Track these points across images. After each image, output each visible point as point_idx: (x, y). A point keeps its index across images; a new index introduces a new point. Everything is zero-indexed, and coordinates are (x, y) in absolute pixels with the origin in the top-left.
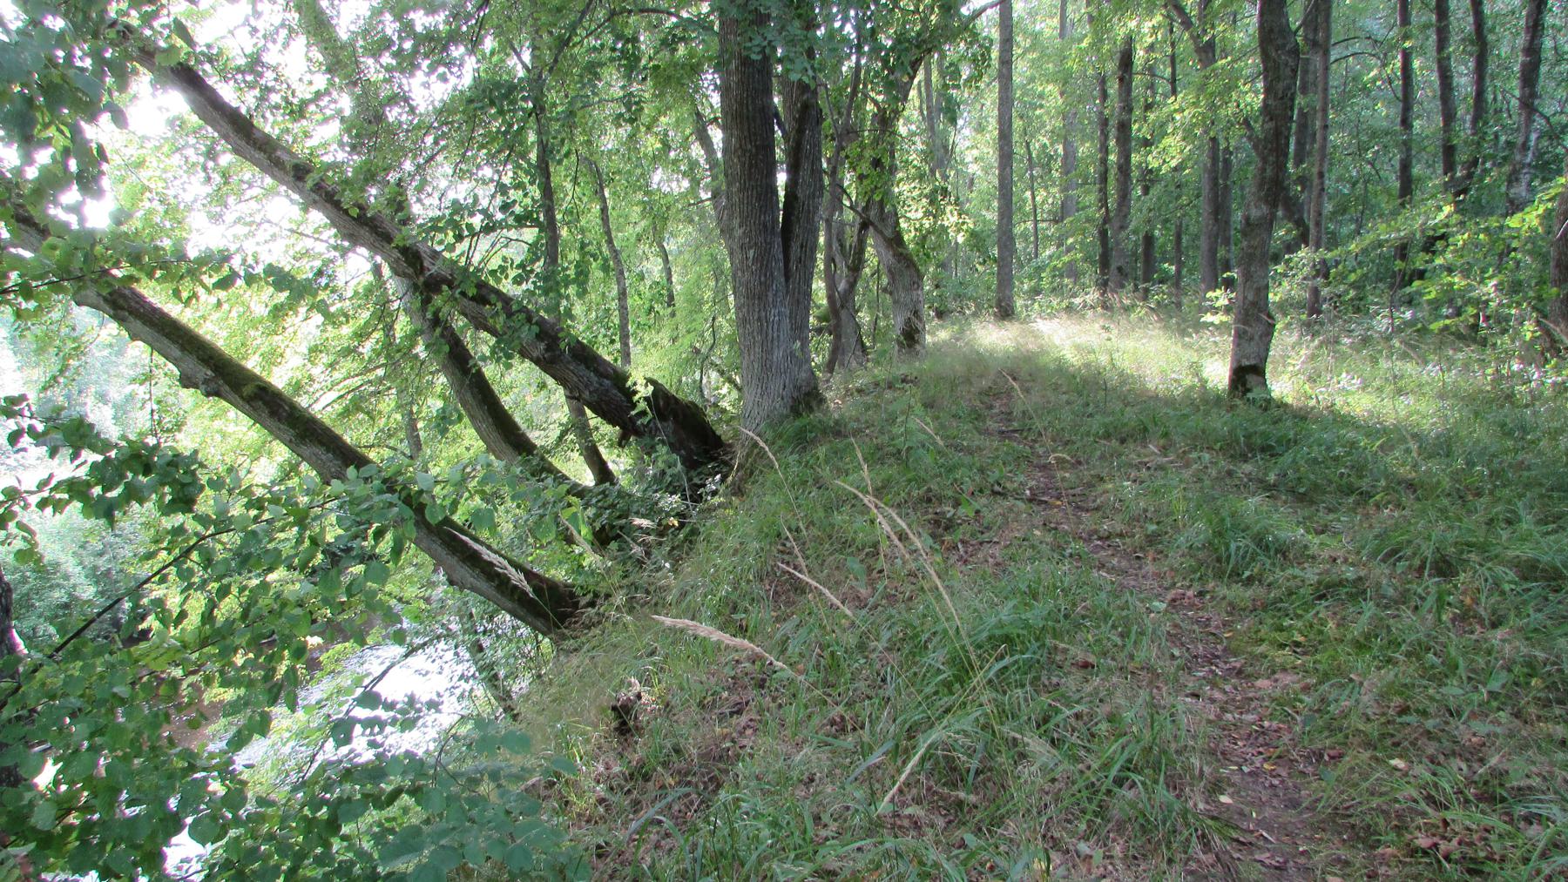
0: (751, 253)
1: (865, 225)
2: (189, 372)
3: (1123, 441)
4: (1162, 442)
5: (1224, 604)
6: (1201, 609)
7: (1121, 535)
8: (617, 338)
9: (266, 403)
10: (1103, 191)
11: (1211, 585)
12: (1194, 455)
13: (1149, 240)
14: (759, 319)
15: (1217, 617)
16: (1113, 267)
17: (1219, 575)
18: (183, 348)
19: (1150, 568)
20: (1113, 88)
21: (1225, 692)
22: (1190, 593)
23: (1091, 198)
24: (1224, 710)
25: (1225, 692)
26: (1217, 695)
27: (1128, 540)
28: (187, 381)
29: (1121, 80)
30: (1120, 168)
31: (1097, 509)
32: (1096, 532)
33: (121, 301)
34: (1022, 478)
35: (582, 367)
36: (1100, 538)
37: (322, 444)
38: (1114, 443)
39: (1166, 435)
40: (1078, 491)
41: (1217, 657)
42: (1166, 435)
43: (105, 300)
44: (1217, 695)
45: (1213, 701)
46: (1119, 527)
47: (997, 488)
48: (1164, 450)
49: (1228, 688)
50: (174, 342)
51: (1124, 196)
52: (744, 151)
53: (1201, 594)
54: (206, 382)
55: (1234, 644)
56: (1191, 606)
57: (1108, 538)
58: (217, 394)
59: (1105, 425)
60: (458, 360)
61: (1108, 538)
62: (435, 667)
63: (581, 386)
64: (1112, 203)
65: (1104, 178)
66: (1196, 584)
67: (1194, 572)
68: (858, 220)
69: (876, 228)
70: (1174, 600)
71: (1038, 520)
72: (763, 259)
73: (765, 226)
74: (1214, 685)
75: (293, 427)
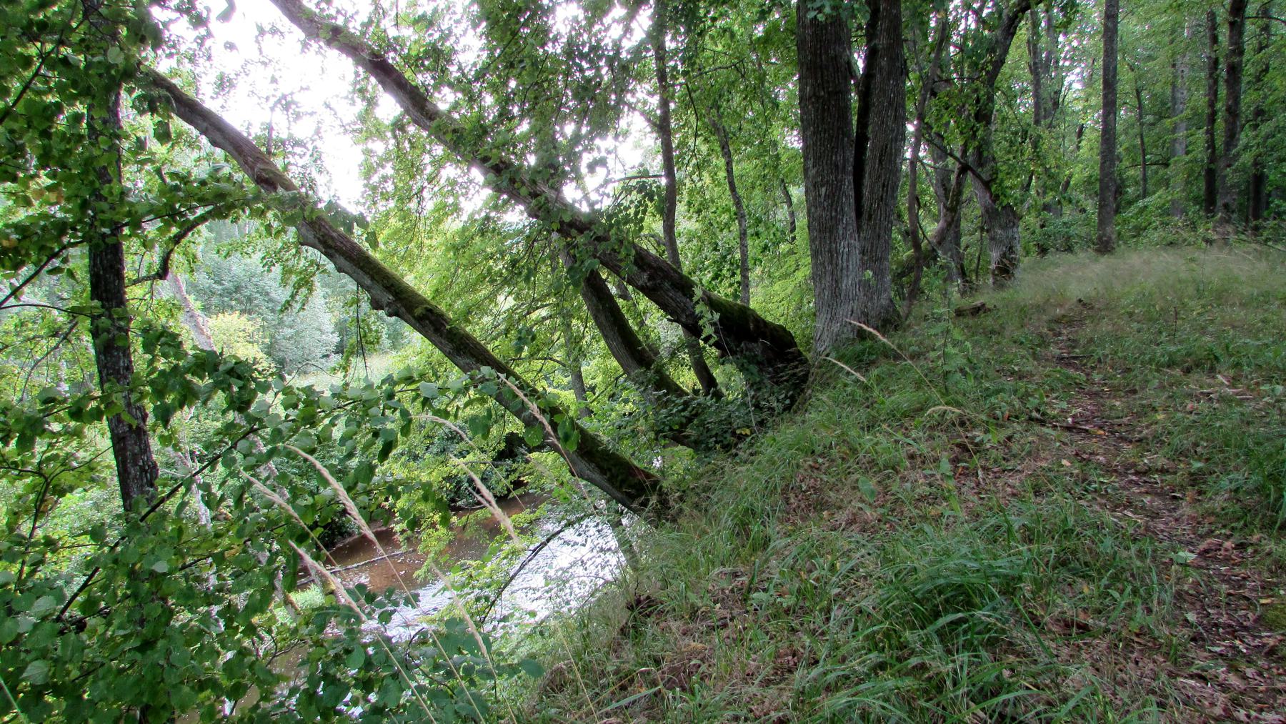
0: (823, 190)
1: (964, 169)
2: (378, 297)
3: (1188, 371)
4: (1232, 372)
5: (1268, 561)
6: (1238, 565)
7: (1163, 471)
8: (738, 272)
9: (431, 322)
10: (1210, 133)
11: (1256, 536)
12: (1266, 387)
13: (1259, 180)
14: (830, 251)
15: (1255, 575)
16: (1220, 203)
17: (1268, 526)
18: (372, 278)
19: (1186, 510)
20: (1224, 34)
21: (1244, 678)
22: (1228, 544)
23: (1201, 135)
24: (1236, 703)
25: (1244, 678)
26: (1233, 680)
27: (1169, 477)
28: (376, 305)
29: (1232, 24)
30: (1229, 110)
31: (1140, 440)
32: (1134, 465)
33: (330, 242)
34: (1064, 405)
35: (680, 294)
36: (1137, 473)
37: (473, 356)
38: (1177, 372)
39: (1237, 365)
40: (1125, 420)
41: (1246, 628)
42: (1237, 365)
43: (320, 241)
44: (1233, 680)
45: (1225, 688)
46: (1161, 462)
47: (1035, 414)
48: (1234, 381)
49: (1250, 672)
50: (367, 273)
51: (1232, 137)
52: (818, 98)
53: (1241, 546)
54: (389, 305)
55: (1271, 614)
56: (1227, 560)
57: (1145, 473)
58: (397, 314)
59: (1170, 355)
60: (596, 290)
61: (1145, 473)
62: (580, 540)
63: (679, 311)
64: (1220, 142)
65: (1212, 119)
66: (1237, 535)
67: (1238, 520)
68: (957, 165)
69: (974, 172)
70: (1206, 551)
71: (1070, 450)
72: (834, 196)
73: (837, 166)
74: (1233, 668)
75: (451, 341)
